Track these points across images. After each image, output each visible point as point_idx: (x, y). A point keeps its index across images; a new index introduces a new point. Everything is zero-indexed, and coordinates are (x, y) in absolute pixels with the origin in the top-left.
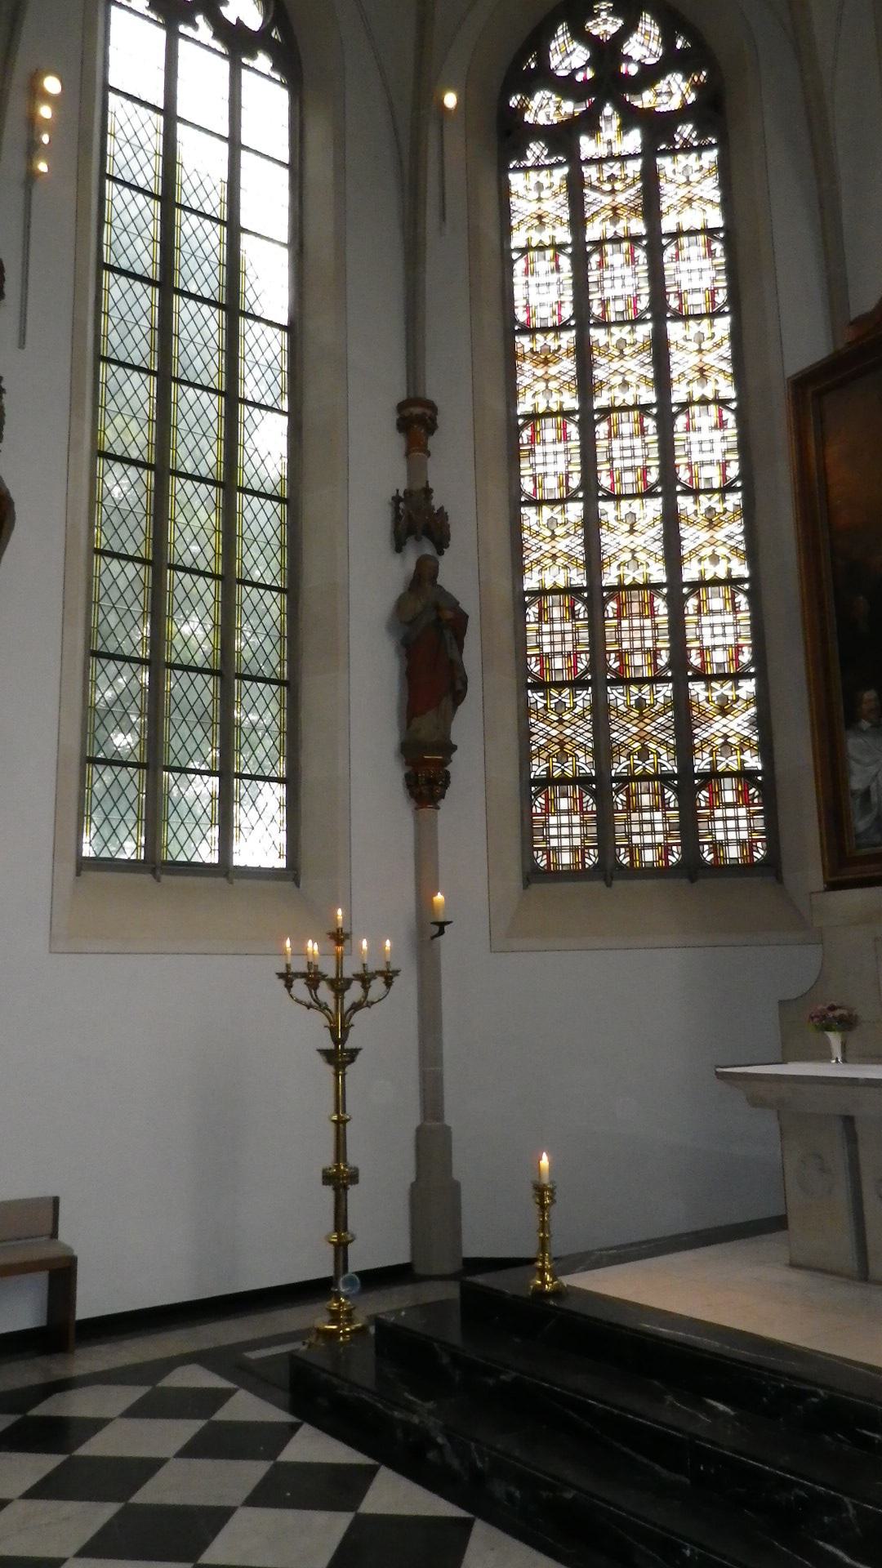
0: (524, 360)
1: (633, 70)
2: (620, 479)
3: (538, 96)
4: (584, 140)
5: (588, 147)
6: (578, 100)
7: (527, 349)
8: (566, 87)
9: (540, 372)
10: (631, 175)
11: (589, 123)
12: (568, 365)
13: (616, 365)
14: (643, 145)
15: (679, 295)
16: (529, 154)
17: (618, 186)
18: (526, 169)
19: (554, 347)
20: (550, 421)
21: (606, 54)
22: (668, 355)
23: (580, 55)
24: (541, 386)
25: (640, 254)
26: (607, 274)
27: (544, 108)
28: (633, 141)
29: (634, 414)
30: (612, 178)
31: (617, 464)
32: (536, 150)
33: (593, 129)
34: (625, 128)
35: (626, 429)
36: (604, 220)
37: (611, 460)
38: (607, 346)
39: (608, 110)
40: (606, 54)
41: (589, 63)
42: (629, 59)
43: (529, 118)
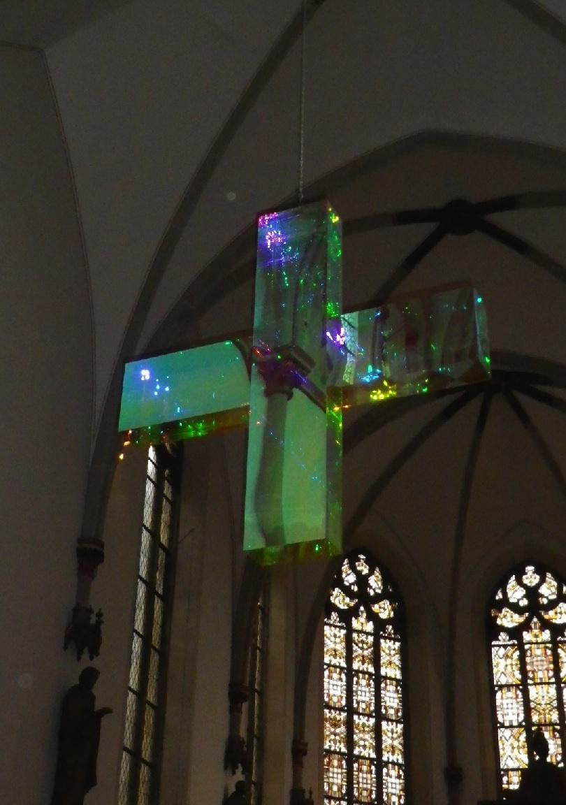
0: (327, 721)
1: (545, 601)
2: (361, 794)
3: (504, 611)
4: (525, 633)
5: (527, 636)
6: (352, 598)
7: (328, 716)
8: (515, 608)
9: (333, 730)
10: (369, 642)
11: (526, 626)
12: (342, 730)
13: (361, 735)
14: (551, 637)
15: (386, 708)
16: (500, 637)
17: (365, 646)
18: (499, 646)
19: (338, 719)
20: (336, 756)
21: (532, 593)
22: (381, 736)
23: (521, 592)
24: (332, 737)
25: (343, 676)
26: (360, 688)
27: (508, 619)
28: (546, 635)
29: (368, 762)
30: (363, 642)
31: (361, 785)
32: (503, 636)
33: (357, 616)
34: (542, 629)
35: (365, 768)
36: (358, 661)
37: (358, 783)
38: (358, 724)
39: (535, 620)
40: (532, 593)
41: (525, 596)
42: (542, 596)
43: (499, 622)
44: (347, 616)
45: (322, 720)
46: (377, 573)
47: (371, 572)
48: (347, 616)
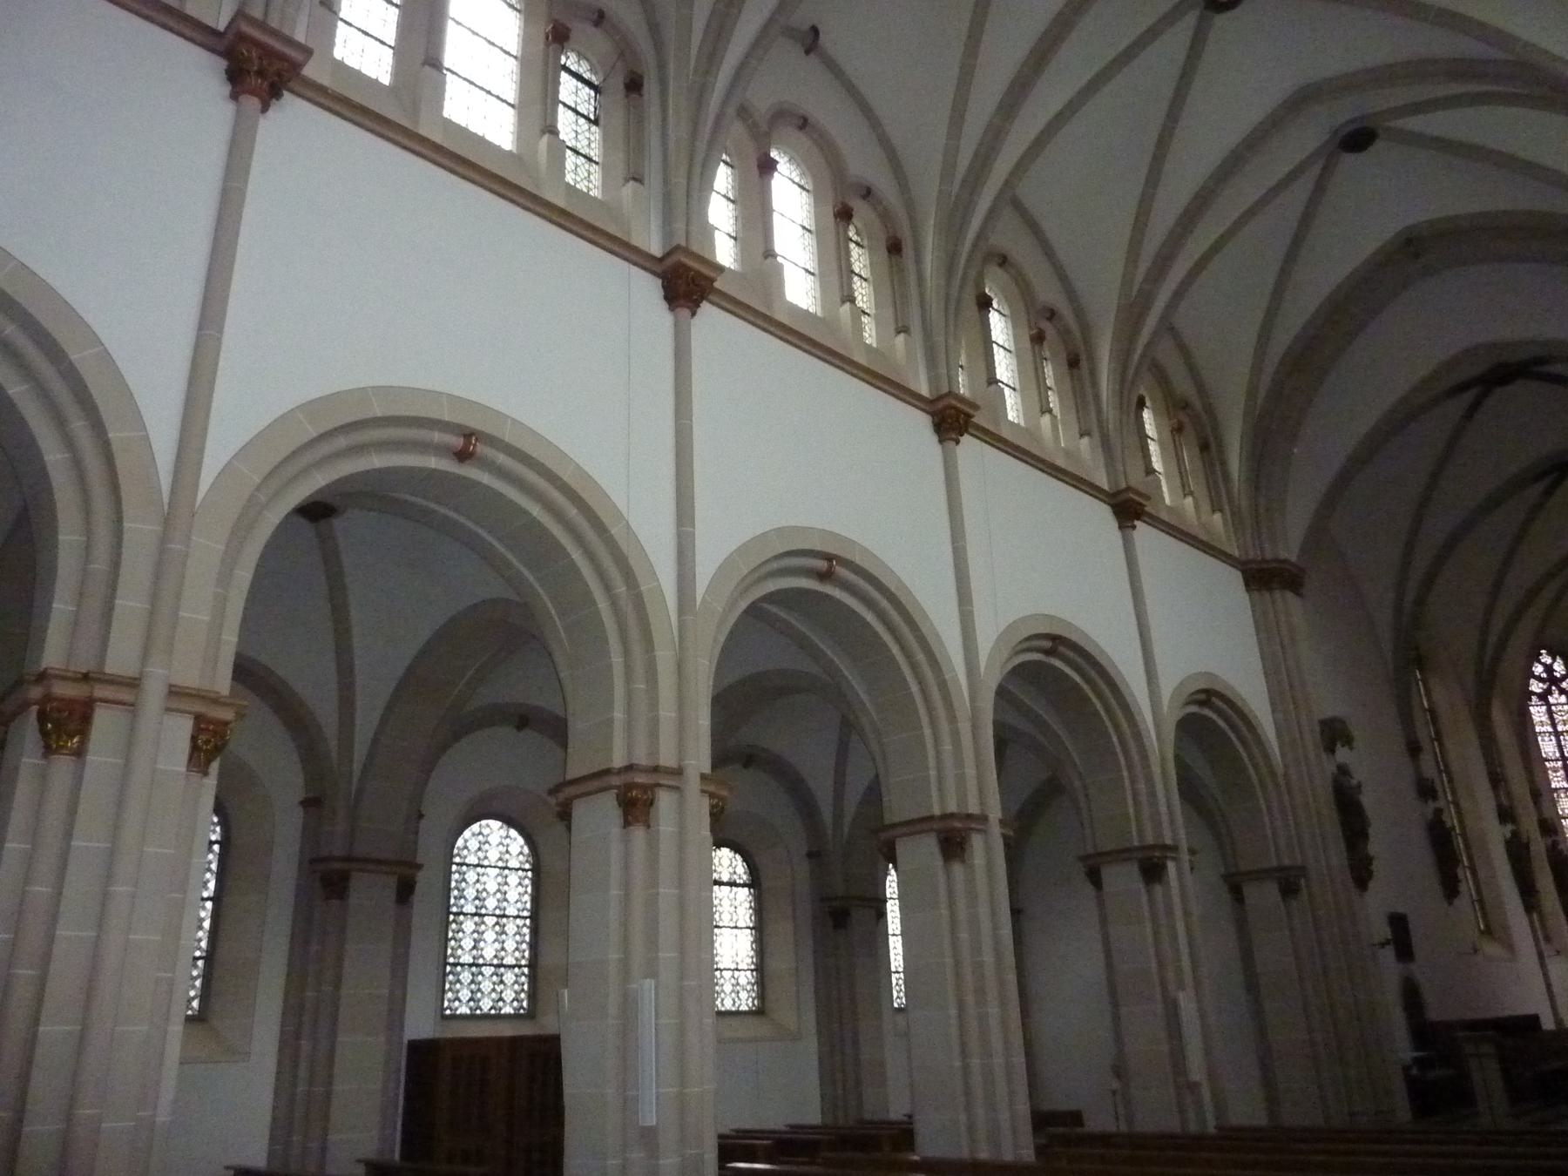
40: (1549, 669)
44: (1543, 697)
45: (1546, 770)
46: (1558, 659)
47: (1554, 660)
48: (1543, 697)
